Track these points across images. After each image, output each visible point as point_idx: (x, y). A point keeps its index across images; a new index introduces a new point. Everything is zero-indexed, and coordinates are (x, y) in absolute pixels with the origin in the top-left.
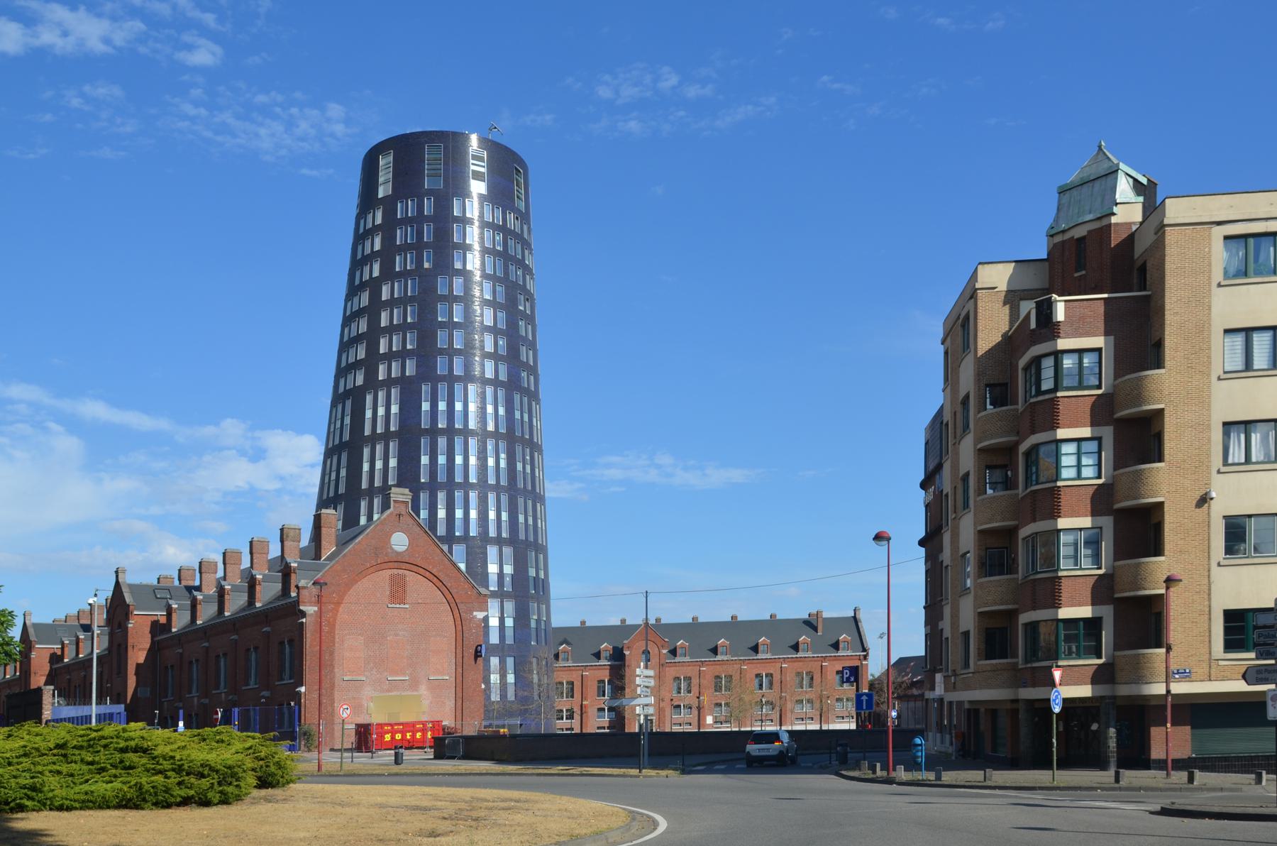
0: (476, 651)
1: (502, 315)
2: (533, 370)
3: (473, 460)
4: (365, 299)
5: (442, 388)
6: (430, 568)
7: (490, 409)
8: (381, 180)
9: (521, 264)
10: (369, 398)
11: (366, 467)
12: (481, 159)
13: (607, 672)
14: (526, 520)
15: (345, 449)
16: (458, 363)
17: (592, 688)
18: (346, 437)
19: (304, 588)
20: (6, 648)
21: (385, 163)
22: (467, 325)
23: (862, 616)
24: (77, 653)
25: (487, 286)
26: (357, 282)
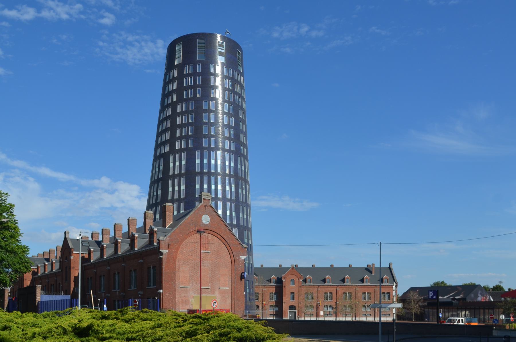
0: (241, 275)
1: (232, 119)
2: (245, 146)
3: (219, 187)
4: (169, 112)
5: (205, 153)
6: (220, 233)
7: (227, 163)
8: (176, 56)
9: (240, 96)
10: (172, 158)
11: (170, 189)
12: (223, 46)
13: (274, 289)
14: (243, 216)
15: (160, 182)
16: (212, 141)
17: (267, 297)
18: (161, 176)
19: (162, 240)
20: (26, 264)
21: (179, 48)
22: (216, 124)
23: (392, 267)
24: (45, 271)
25: (226, 105)
26: (166, 104)
